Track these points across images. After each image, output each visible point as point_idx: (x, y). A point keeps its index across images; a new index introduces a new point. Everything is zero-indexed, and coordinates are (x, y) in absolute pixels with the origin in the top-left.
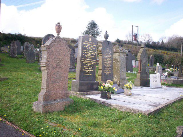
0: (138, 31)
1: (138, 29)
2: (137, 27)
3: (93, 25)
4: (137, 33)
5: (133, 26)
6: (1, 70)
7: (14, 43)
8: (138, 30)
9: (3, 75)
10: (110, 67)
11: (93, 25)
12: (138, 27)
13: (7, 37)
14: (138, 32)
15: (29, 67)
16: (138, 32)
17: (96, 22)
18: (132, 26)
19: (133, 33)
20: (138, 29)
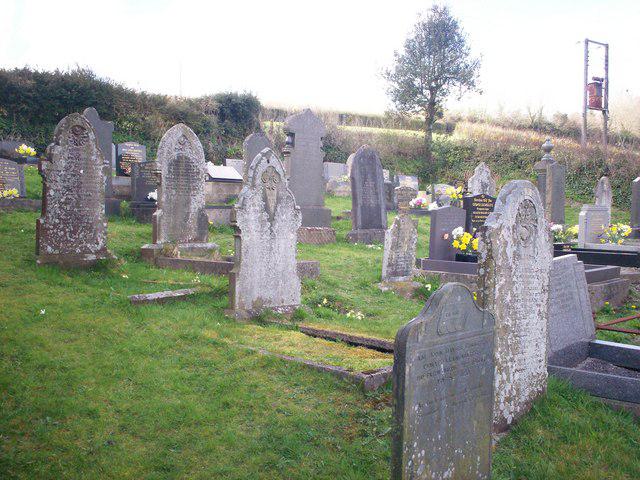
0: (607, 65)
1: (607, 57)
2: (604, 48)
3: (440, 36)
4: (602, 75)
5: (587, 42)
6: (411, 478)
7: (78, 131)
8: (607, 61)
9: (5, 145)
10: (475, 209)
11: (440, 36)
12: (607, 46)
13: (12, 89)
14: (607, 70)
15: (410, 112)
16: (607, 70)
17: (455, 14)
18: (583, 44)
19: (586, 74)
20: (607, 57)
